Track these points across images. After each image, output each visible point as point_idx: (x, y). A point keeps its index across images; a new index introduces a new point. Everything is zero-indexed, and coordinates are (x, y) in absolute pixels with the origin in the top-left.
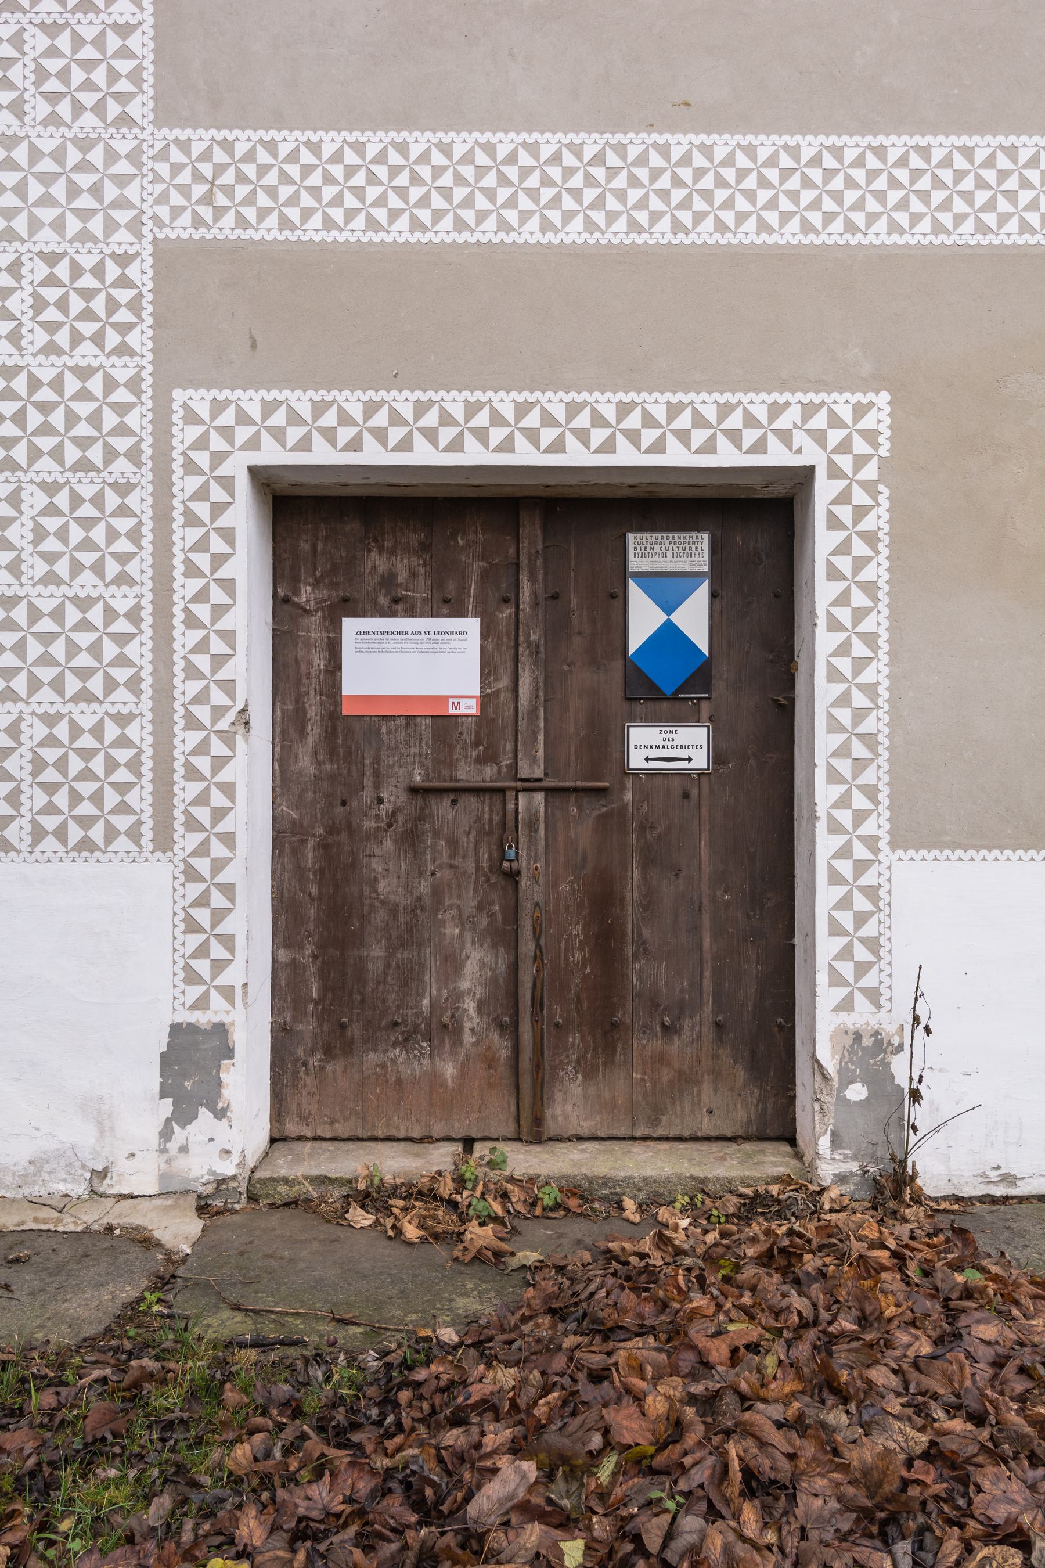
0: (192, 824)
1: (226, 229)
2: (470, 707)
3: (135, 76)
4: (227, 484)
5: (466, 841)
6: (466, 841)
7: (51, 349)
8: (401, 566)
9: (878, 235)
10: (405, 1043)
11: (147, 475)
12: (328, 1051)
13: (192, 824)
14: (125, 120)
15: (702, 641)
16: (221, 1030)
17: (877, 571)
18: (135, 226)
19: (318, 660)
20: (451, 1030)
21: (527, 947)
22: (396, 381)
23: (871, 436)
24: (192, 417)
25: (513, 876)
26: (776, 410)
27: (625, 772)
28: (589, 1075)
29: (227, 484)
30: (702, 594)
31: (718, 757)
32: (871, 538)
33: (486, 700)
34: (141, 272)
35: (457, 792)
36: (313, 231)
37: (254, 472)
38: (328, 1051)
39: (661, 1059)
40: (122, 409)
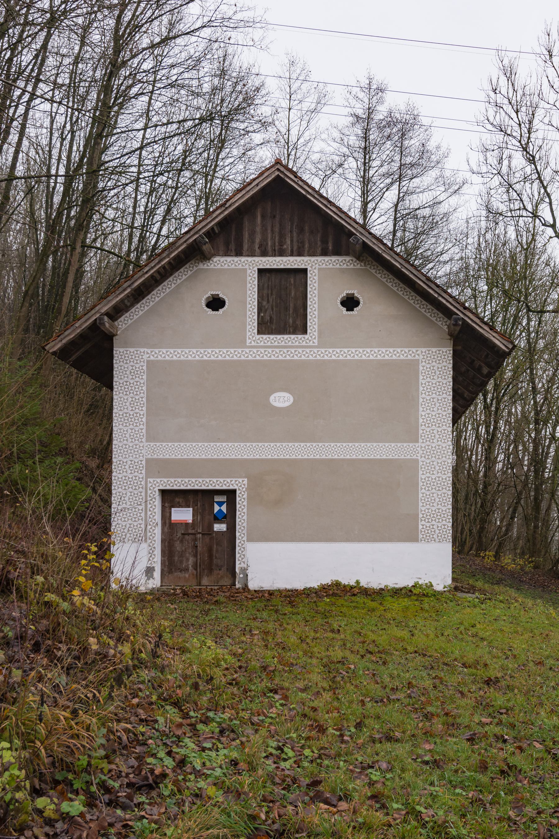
0: (150, 539)
1: (155, 456)
2: (191, 521)
3: (143, 436)
4: (155, 492)
5: (190, 541)
6: (190, 541)
7: (131, 473)
8: (181, 500)
9: (245, 457)
10: (181, 571)
11: (144, 490)
12: (169, 573)
13: (150, 539)
14: (142, 442)
15: (225, 512)
16: (154, 567)
17: (245, 503)
18: (143, 456)
19: (168, 514)
20: (187, 570)
21: (199, 557)
22: (179, 477)
23: (244, 485)
24: (150, 482)
25: (197, 547)
26: (231, 481)
27: (214, 531)
28: (208, 576)
29: (155, 492)
30: (225, 505)
31: (227, 529)
32: (244, 499)
33: (193, 520)
34: (144, 462)
35: (189, 534)
36: (167, 457)
37: (159, 490)
38: (169, 573)
39: (218, 574)
40: (141, 481)
